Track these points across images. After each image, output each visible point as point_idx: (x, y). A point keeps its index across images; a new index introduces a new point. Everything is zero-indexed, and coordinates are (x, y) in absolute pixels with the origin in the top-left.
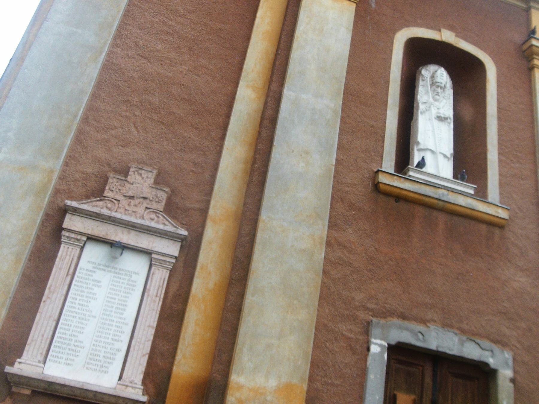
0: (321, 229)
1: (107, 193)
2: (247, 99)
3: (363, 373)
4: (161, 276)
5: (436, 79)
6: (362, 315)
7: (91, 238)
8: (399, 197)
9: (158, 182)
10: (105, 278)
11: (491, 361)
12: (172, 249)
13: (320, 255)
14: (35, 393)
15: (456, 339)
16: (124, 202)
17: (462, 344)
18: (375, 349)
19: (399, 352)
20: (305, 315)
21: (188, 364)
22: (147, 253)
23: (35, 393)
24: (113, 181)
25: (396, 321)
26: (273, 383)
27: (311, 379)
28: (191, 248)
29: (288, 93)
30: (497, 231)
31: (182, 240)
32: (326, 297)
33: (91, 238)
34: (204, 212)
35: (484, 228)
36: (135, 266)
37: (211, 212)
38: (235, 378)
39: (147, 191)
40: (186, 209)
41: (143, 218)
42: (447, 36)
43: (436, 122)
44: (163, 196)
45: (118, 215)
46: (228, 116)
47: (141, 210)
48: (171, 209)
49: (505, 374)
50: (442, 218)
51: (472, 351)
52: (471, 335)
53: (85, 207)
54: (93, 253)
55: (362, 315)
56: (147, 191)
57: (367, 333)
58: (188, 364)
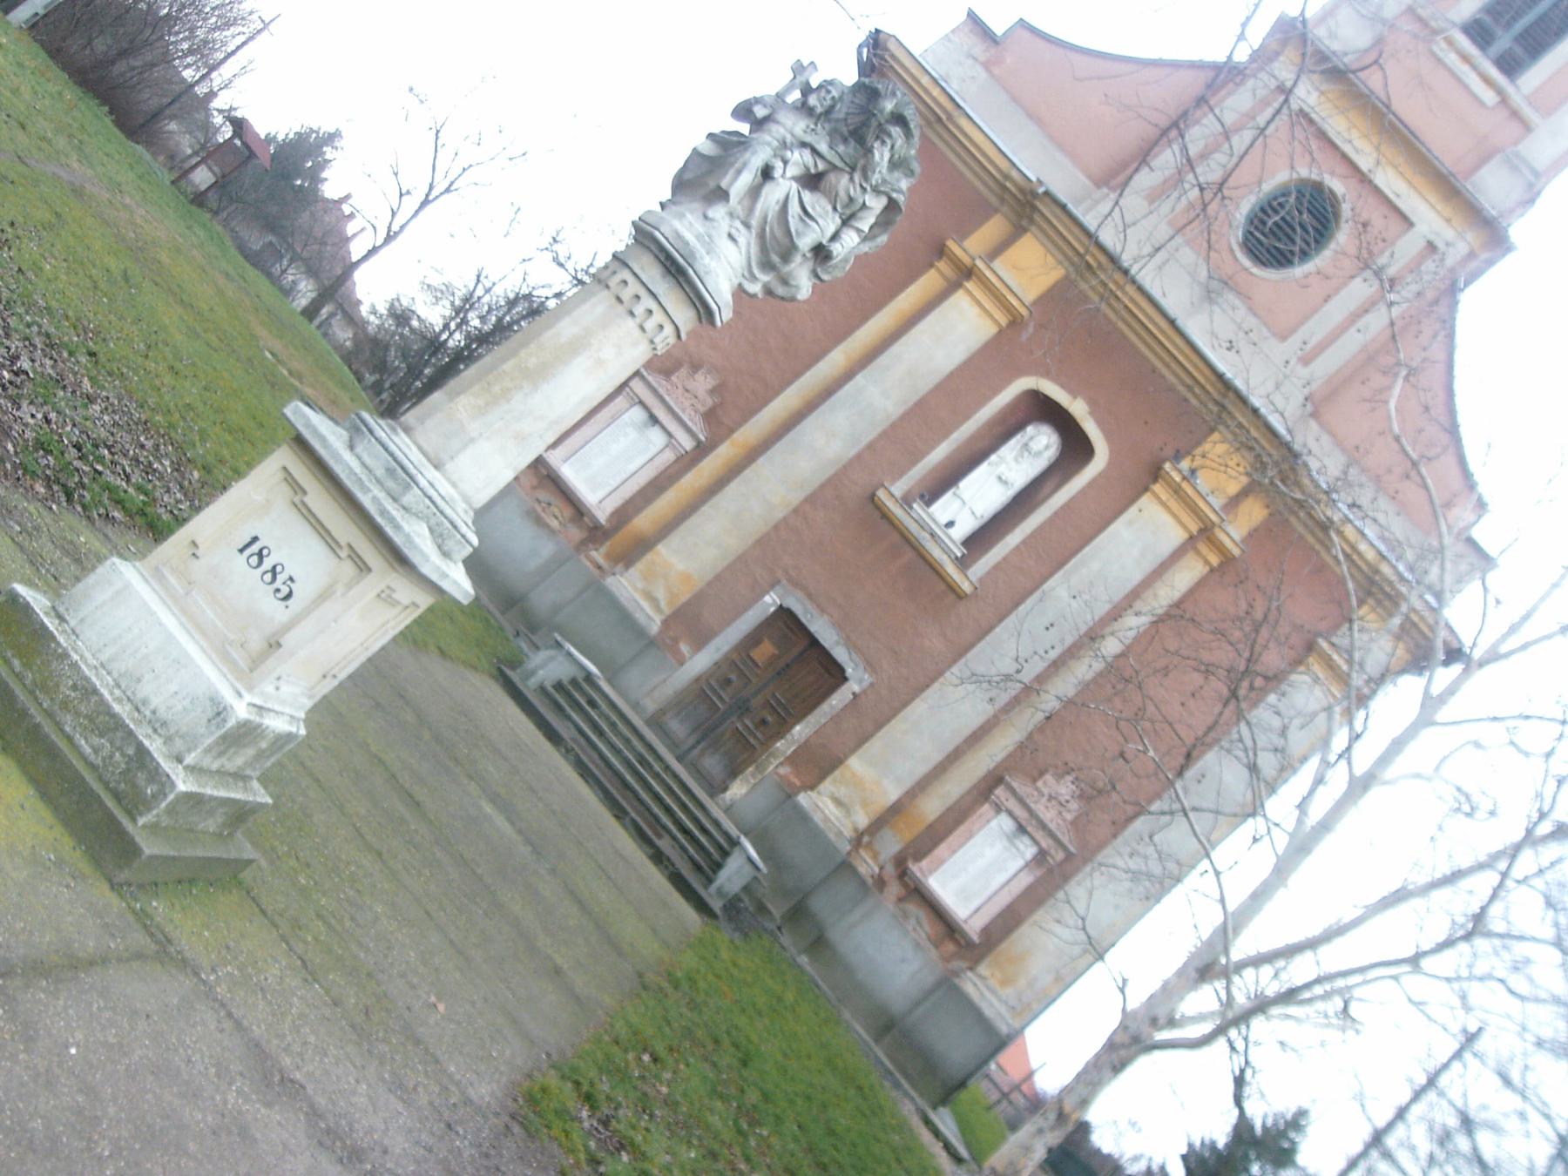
0: (796, 498)
1: (674, 378)
2: (836, 359)
3: (746, 609)
4: (669, 456)
5: (1043, 442)
6: (779, 573)
7: (641, 403)
8: (886, 516)
9: (712, 392)
10: (633, 434)
11: (849, 671)
12: (687, 443)
13: (779, 514)
14: (548, 476)
15: (835, 638)
16: (681, 390)
17: (837, 643)
18: (767, 599)
19: (784, 613)
20: (735, 544)
21: (643, 522)
22: (670, 435)
23: (548, 476)
24: (683, 372)
25: (800, 594)
26: (681, 567)
27: (709, 584)
28: (702, 450)
29: (859, 379)
30: (953, 597)
31: (699, 442)
32: (762, 542)
33: (641, 403)
34: (732, 431)
35: (943, 586)
36: (656, 438)
37: (735, 435)
38: (660, 548)
39: (701, 393)
40: (719, 422)
41: (684, 410)
42: (1078, 408)
43: (993, 479)
44: (709, 402)
45: (667, 398)
46: (808, 367)
47: (687, 404)
48: (710, 416)
49: (853, 686)
50: (909, 555)
51: (840, 654)
52: (850, 645)
53: (650, 379)
54: (637, 414)
55: (779, 573)
56: (701, 393)
57: (772, 586)
58: (643, 522)
